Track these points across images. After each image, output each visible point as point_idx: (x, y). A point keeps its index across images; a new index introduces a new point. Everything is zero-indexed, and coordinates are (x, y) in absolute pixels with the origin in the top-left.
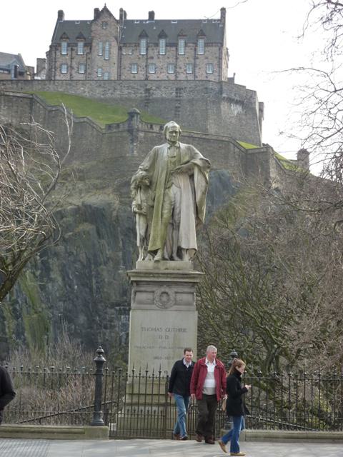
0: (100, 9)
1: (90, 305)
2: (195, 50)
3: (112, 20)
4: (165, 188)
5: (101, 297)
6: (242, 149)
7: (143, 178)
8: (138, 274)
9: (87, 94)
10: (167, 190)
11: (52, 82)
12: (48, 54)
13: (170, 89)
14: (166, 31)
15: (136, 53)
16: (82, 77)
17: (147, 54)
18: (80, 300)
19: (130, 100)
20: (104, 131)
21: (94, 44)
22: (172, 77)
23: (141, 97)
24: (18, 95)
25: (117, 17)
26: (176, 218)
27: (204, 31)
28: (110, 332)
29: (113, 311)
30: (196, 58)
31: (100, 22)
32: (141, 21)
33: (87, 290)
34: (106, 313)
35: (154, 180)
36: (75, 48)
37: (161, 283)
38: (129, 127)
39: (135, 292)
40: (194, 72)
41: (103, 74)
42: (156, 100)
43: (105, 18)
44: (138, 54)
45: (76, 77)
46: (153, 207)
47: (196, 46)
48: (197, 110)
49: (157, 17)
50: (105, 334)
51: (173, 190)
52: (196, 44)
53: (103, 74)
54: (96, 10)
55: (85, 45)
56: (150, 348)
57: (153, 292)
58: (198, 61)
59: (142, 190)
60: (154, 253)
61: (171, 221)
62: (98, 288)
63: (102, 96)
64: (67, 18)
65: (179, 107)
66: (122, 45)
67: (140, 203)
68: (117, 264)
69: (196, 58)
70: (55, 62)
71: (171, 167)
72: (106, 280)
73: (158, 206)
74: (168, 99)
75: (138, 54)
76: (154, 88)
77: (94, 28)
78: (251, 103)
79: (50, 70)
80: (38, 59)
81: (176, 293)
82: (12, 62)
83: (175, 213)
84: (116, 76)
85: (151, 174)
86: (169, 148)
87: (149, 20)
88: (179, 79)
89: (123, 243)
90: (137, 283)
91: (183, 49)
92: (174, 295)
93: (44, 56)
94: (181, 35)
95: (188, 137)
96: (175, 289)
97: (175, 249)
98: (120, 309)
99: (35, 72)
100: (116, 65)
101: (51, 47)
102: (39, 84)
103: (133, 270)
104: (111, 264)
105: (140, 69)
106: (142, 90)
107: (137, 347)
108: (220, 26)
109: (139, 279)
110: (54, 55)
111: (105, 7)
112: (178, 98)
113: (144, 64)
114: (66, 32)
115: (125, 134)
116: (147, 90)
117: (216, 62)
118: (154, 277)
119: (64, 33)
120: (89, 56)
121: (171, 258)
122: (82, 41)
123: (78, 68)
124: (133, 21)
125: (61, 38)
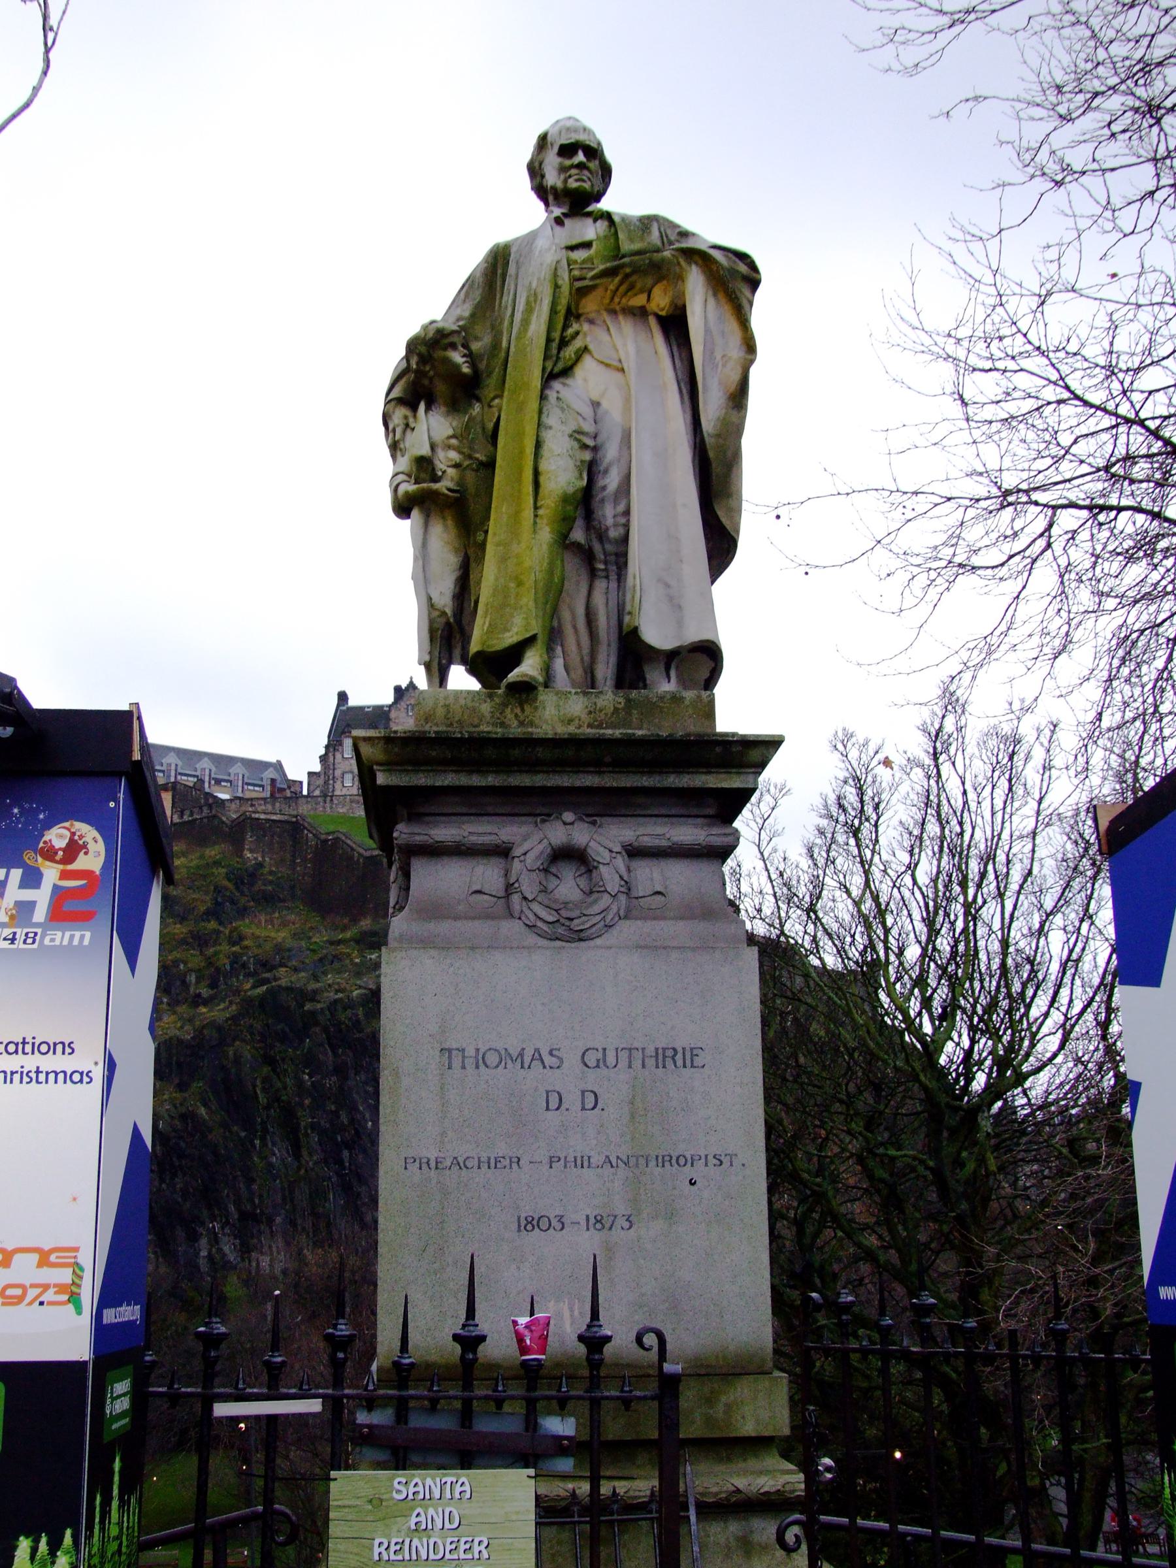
4: (550, 377)
10: (556, 385)
12: (323, 759)
24: (274, 817)
26: (608, 514)
31: (403, 705)
46: (489, 466)
54: (398, 689)
56: (495, 1163)
57: (502, 852)
64: (353, 702)
67: (425, 451)
77: (393, 715)
81: (634, 852)
82: (270, 774)
92: (620, 863)
93: (317, 767)
99: (305, 792)
101: (327, 747)
102: (307, 802)
107: (424, 1164)
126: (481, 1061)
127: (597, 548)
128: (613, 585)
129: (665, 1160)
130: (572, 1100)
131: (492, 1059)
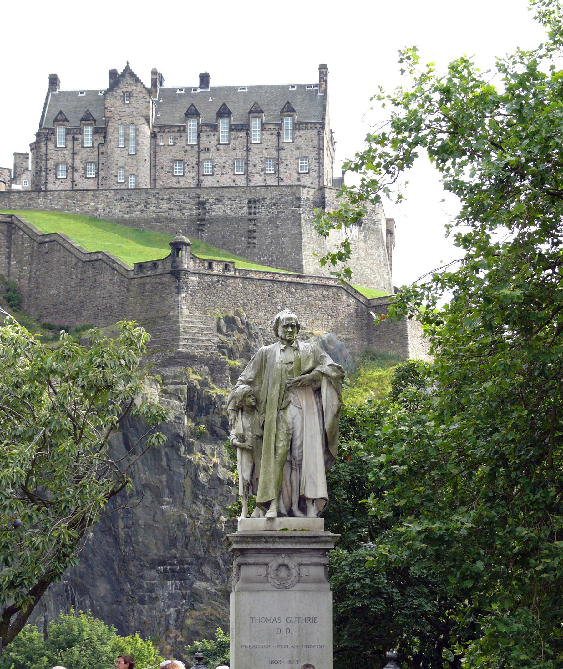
0: (120, 71)
1: (116, 564)
2: (279, 135)
3: (139, 88)
4: (279, 410)
5: (134, 551)
6: (361, 299)
7: (245, 395)
8: (243, 538)
9: (100, 212)
11: (42, 193)
12: (35, 147)
13: (237, 201)
14: (230, 106)
15: (181, 143)
16: (91, 185)
17: (198, 144)
18: (98, 557)
19: (172, 220)
20: (131, 275)
21: (110, 130)
22: (241, 181)
23: (191, 215)
25: (149, 85)
26: (296, 452)
27: (292, 105)
28: (151, 609)
29: (153, 573)
30: (279, 149)
31: (119, 92)
32: (188, 90)
33: (111, 540)
34: (142, 577)
35: (262, 398)
36: (79, 136)
37: (278, 552)
38: (173, 267)
39: (239, 566)
40: (277, 172)
41: (126, 178)
42: (217, 219)
43: (126, 86)
44: (184, 144)
45: (82, 184)
46: (262, 437)
47: (281, 129)
48: (285, 236)
49: (213, 83)
50: (140, 612)
51: (292, 411)
52: (279, 125)
53: (126, 178)
54: (113, 74)
55: (96, 131)
56: (264, 647)
58: (283, 154)
59: (244, 413)
60: (266, 506)
61: (288, 458)
62: (128, 536)
63: (126, 216)
64: (64, 86)
65: (254, 231)
66: (156, 130)
67: (241, 432)
68: (158, 496)
69: (279, 149)
70: (47, 160)
71: (287, 379)
72: (141, 522)
73: (269, 435)
74: (236, 218)
75: (184, 144)
76: (211, 200)
77: (109, 102)
78: (374, 221)
79: (38, 173)
80: (15, 154)
81: (300, 565)
83: (294, 447)
84: (148, 181)
85: (257, 388)
86: (283, 350)
87: (200, 87)
88: (251, 185)
89: (168, 459)
90: (242, 552)
91: (258, 133)
94: (256, 111)
95: (272, 281)
96: (298, 559)
97: (295, 499)
98: (165, 570)
100: (148, 163)
101: (38, 135)
102: (21, 198)
103: (236, 533)
104: (148, 497)
105: (187, 170)
106: (193, 204)
107: (246, 647)
108: (319, 94)
109: (244, 546)
110: (43, 149)
111: (128, 68)
112: (253, 216)
113: (194, 160)
114: (63, 111)
115: (166, 279)
116: (201, 204)
117: (313, 154)
118: (267, 542)
119: (61, 113)
120: (102, 149)
121: (291, 514)
122: (90, 124)
123: (85, 169)
124: (174, 90)
125: (56, 120)
126: (260, 621)
127: (293, 461)
128: (298, 473)
129: (306, 647)
130: (284, 631)
131: (263, 620)
